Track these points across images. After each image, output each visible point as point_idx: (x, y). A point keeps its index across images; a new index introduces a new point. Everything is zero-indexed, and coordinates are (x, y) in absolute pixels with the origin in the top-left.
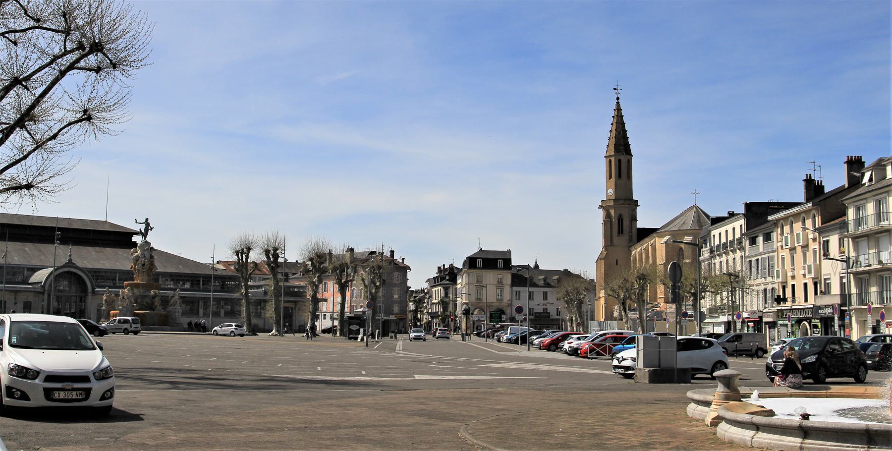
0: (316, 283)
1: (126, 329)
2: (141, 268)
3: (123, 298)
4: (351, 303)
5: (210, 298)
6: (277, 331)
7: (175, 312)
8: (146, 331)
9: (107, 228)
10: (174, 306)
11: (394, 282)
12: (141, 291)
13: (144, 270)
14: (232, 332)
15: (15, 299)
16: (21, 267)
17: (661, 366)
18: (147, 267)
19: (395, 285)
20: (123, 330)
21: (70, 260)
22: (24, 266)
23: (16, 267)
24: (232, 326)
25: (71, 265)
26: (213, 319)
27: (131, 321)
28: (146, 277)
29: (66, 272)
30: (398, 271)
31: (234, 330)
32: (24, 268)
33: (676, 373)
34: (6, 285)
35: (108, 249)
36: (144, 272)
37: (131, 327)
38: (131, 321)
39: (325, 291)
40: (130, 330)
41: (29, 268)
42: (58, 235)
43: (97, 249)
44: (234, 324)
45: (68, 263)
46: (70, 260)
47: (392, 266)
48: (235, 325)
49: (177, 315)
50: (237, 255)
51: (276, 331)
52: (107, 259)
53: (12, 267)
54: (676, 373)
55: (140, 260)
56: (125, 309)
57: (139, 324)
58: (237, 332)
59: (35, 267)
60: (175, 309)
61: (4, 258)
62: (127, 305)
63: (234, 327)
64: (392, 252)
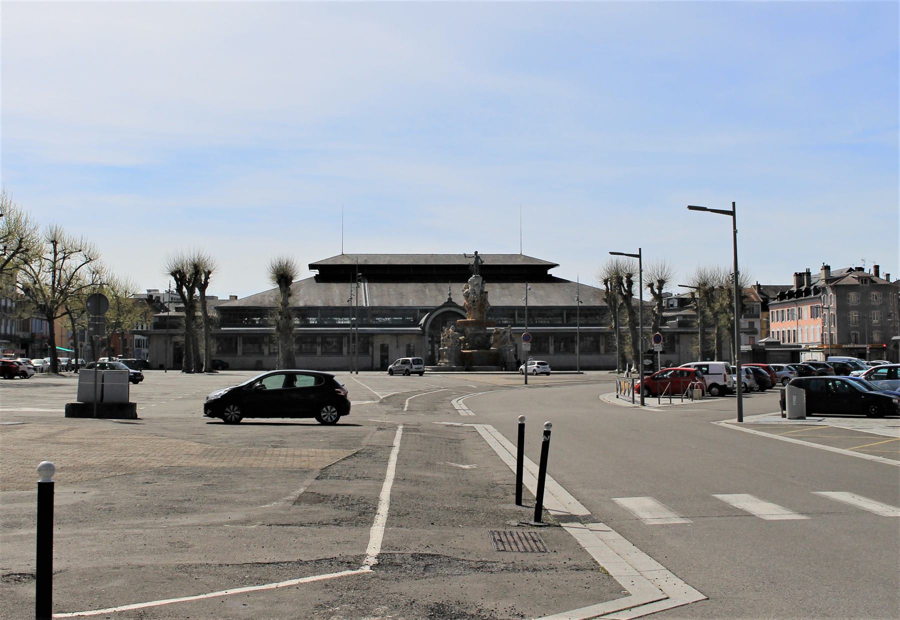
0: (656, 313)
1: (407, 370)
2: (471, 306)
3: (448, 337)
4: (823, 332)
5: (577, 333)
6: (637, 368)
7: (505, 350)
8: (488, 371)
9: (519, 262)
10: (505, 344)
11: (872, 303)
12: (473, 329)
13: (476, 307)
14: (534, 370)
15: (397, 342)
16: (414, 309)
17: (104, 401)
18: (477, 304)
19: (874, 308)
20: (405, 371)
21: (450, 299)
22: (417, 308)
23: (408, 309)
24: (534, 364)
25: (451, 304)
26: (580, 356)
27: (411, 362)
28: (478, 315)
29: (446, 312)
30: (877, 291)
31: (536, 368)
32: (417, 309)
33: (95, 407)
34: (528, 328)
35: (516, 285)
36: (475, 309)
37: (412, 368)
38: (411, 362)
39: (799, 318)
40: (410, 371)
41: (422, 309)
42: (359, 276)
43: (504, 285)
44: (536, 362)
45: (447, 302)
46: (450, 299)
47: (868, 285)
48: (538, 363)
49: (508, 353)
50: (606, 284)
51: (635, 368)
52: (511, 295)
53: (405, 309)
54: (95, 407)
55: (470, 296)
56: (450, 349)
57: (422, 364)
58: (538, 371)
59: (428, 308)
60: (506, 347)
61: (350, 302)
62: (452, 345)
63: (536, 365)
64: (877, 268)
